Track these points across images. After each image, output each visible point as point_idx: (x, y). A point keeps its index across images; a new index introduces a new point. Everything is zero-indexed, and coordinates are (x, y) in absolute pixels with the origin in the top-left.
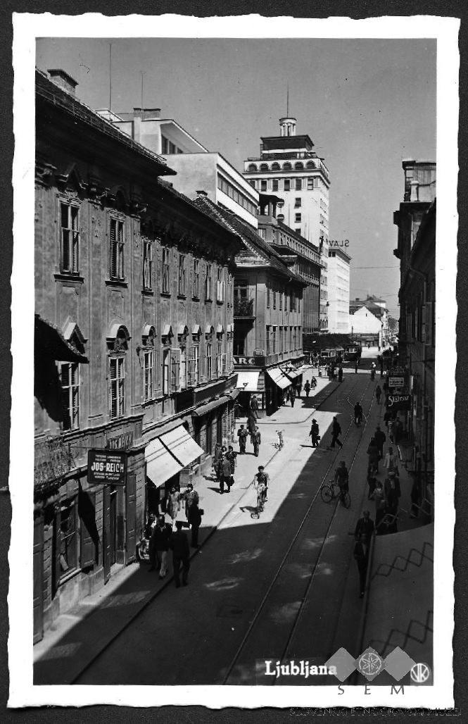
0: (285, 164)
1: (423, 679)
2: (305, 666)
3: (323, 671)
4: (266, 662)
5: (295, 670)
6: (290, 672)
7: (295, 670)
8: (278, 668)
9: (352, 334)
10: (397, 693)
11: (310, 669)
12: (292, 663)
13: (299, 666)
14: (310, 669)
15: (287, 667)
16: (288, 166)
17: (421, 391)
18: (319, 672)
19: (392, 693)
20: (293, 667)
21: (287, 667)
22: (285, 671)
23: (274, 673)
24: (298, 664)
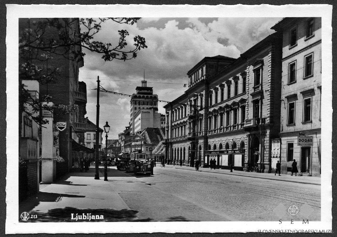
0: (146, 96)
1: (26, 219)
2: (89, 215)
3: (80, 217)
4: (72, 214)
5: (85, 217)
6: (82, 218)
7: (85, 217)
8: (77, 216)
9: (269, 154)
10: (305, 223)
11: (91, 217)
12: (83, 214)
13: (87, 215)
14: (91, 217)
15: (81, 216)
16: (147, 97)
17: (169, 139)
18: (95, 218)
19: (303, 223)
20: (84, 216)
21: (81, 216)
22: (98, 218)
23: (75, 219)
24: (86, 214)
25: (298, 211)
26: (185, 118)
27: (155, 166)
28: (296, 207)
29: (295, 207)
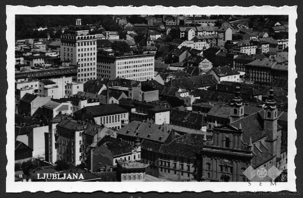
4: (44, 174)
10: (273, 185)
19: (271, 185)
25: (266, 174)
26: (20, 126)
27: (80, 141)
28: (264, 170)
29: (264, 170)
